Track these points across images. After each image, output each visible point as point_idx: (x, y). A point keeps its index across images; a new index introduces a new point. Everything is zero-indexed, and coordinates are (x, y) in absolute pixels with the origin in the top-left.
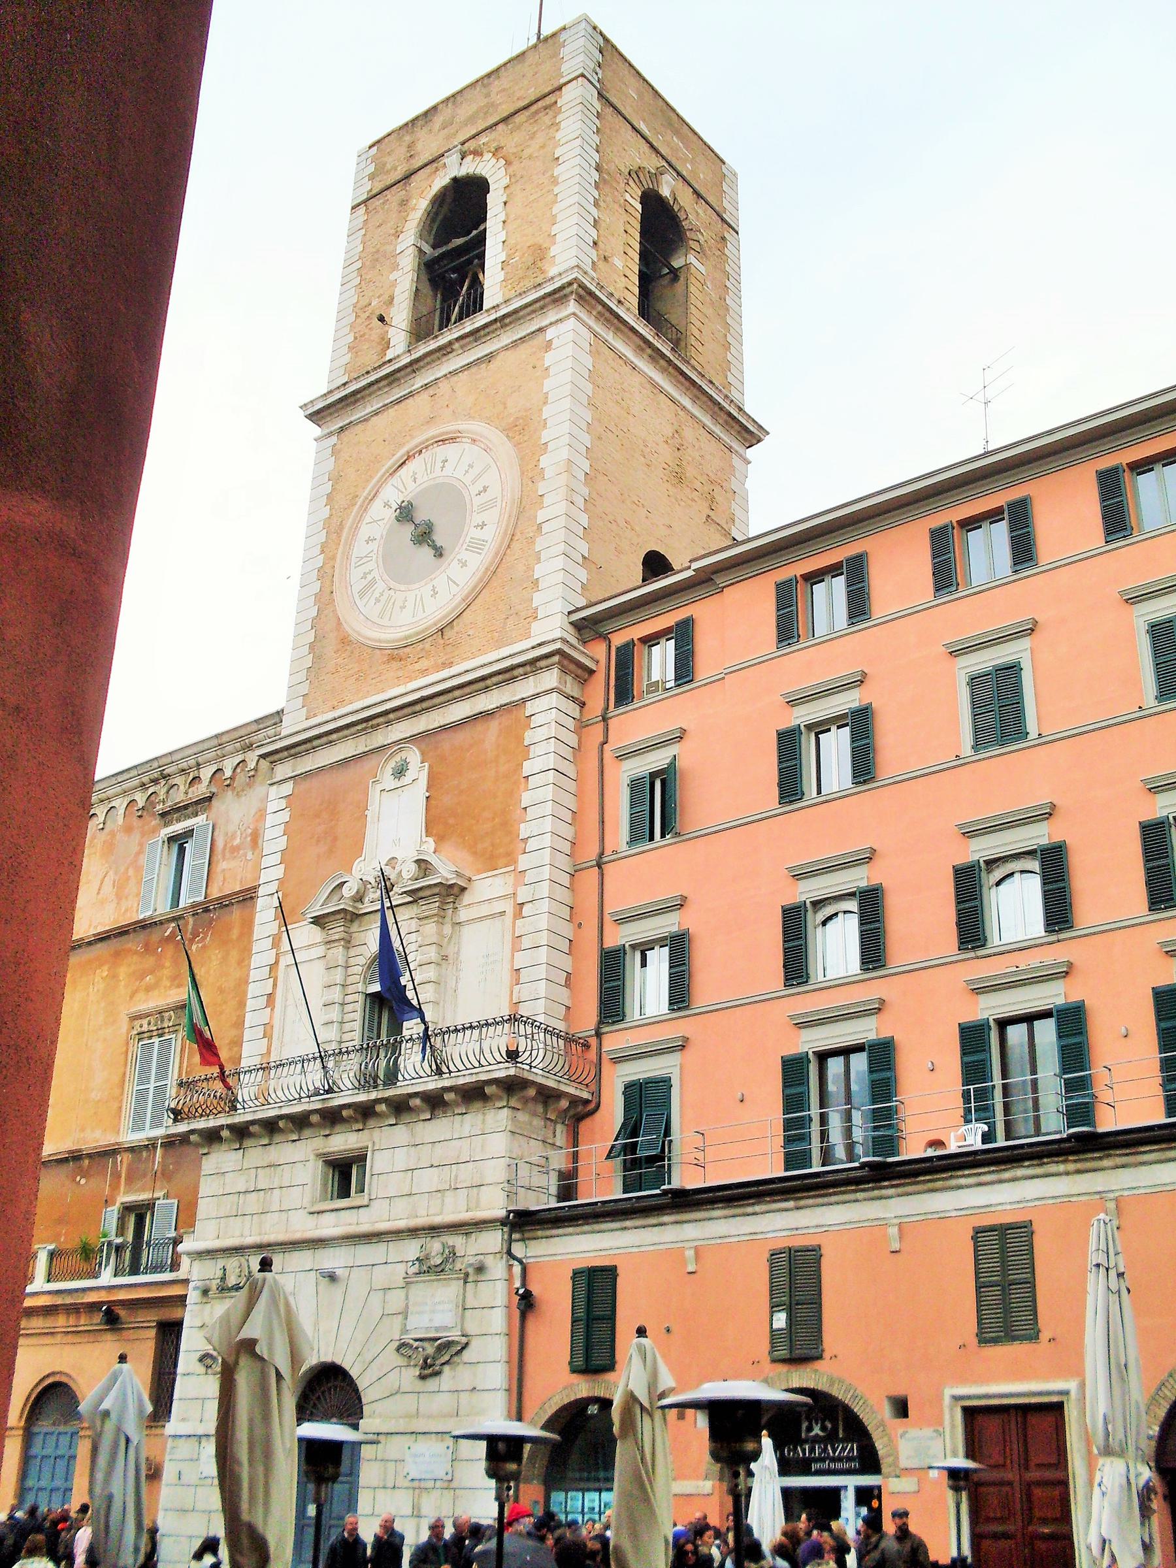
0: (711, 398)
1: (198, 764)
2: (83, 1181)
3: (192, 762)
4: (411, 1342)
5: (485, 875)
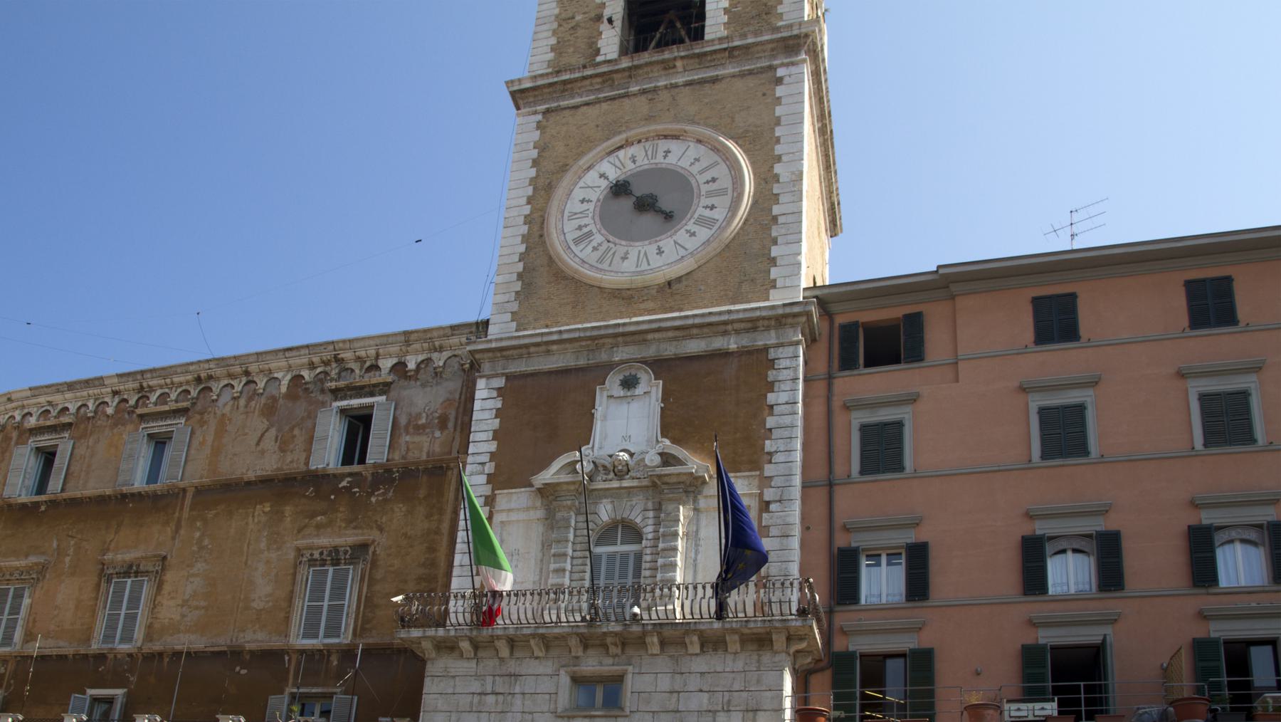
3: (372, 352)
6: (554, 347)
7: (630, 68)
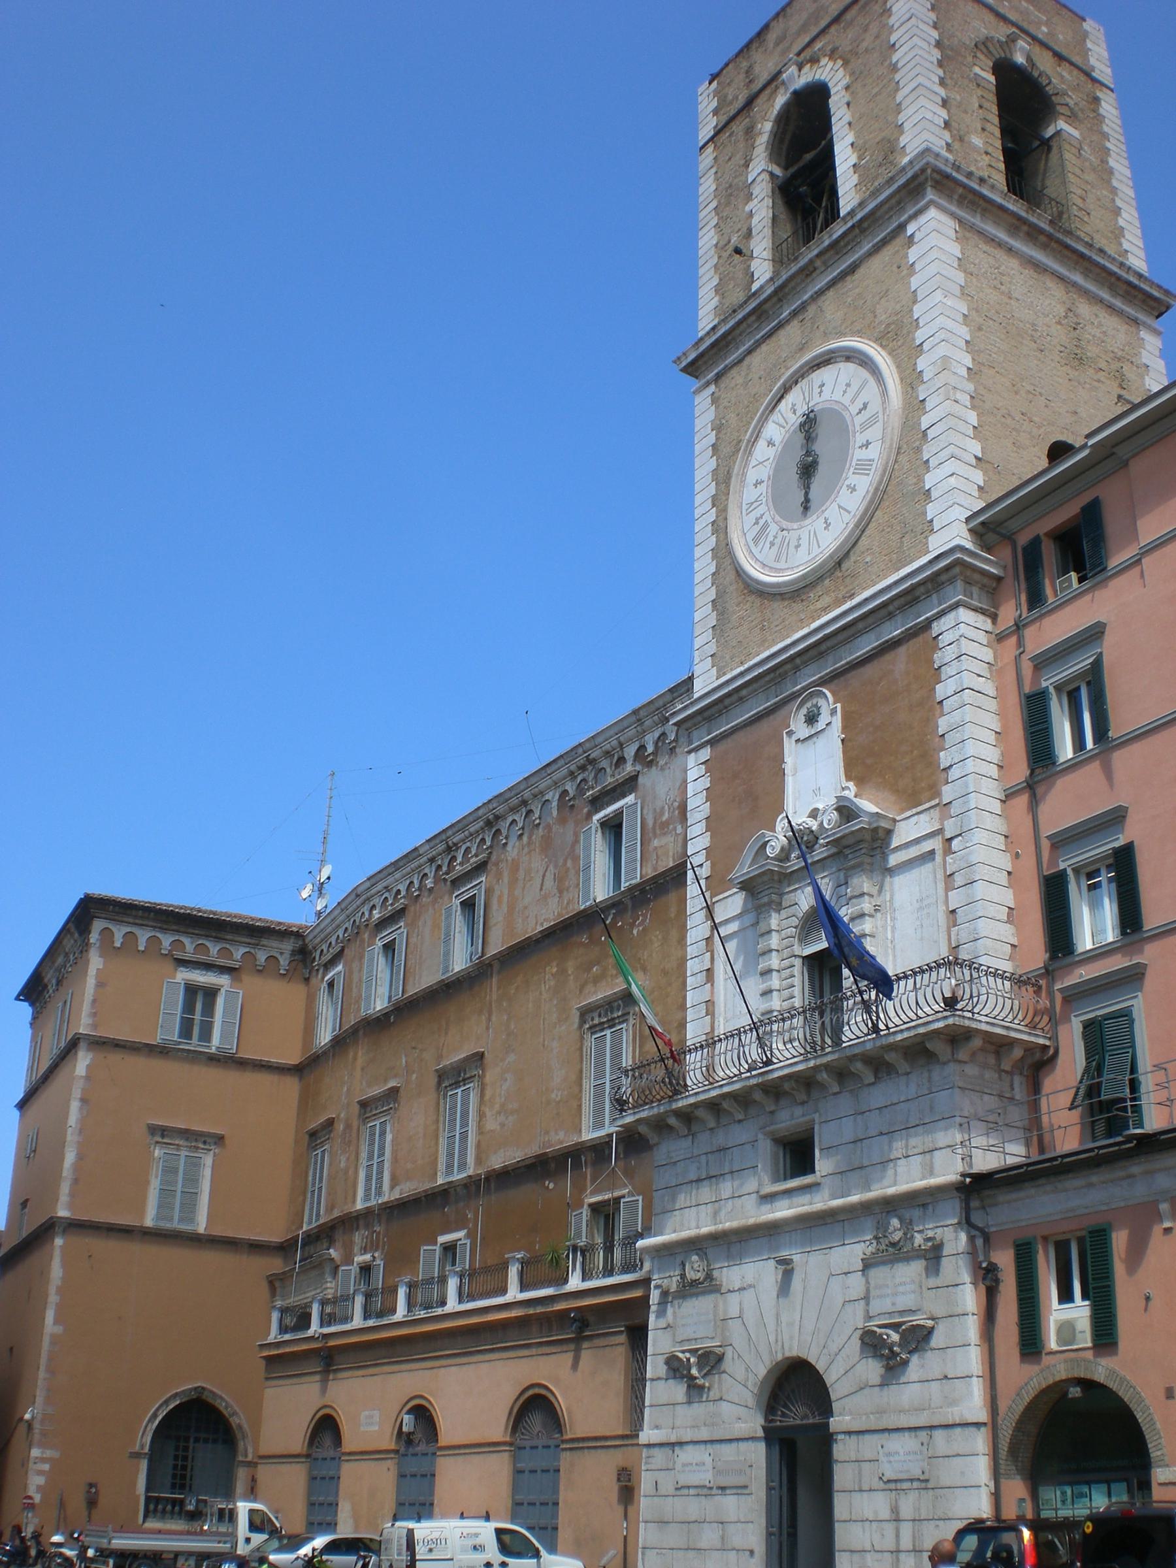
0: (1104, 268)
1: (621, 745)
2: (551, 1186)
4: (875, 1329)
5: (909, 813)
6: (744, 692)
7: (776, 292)
